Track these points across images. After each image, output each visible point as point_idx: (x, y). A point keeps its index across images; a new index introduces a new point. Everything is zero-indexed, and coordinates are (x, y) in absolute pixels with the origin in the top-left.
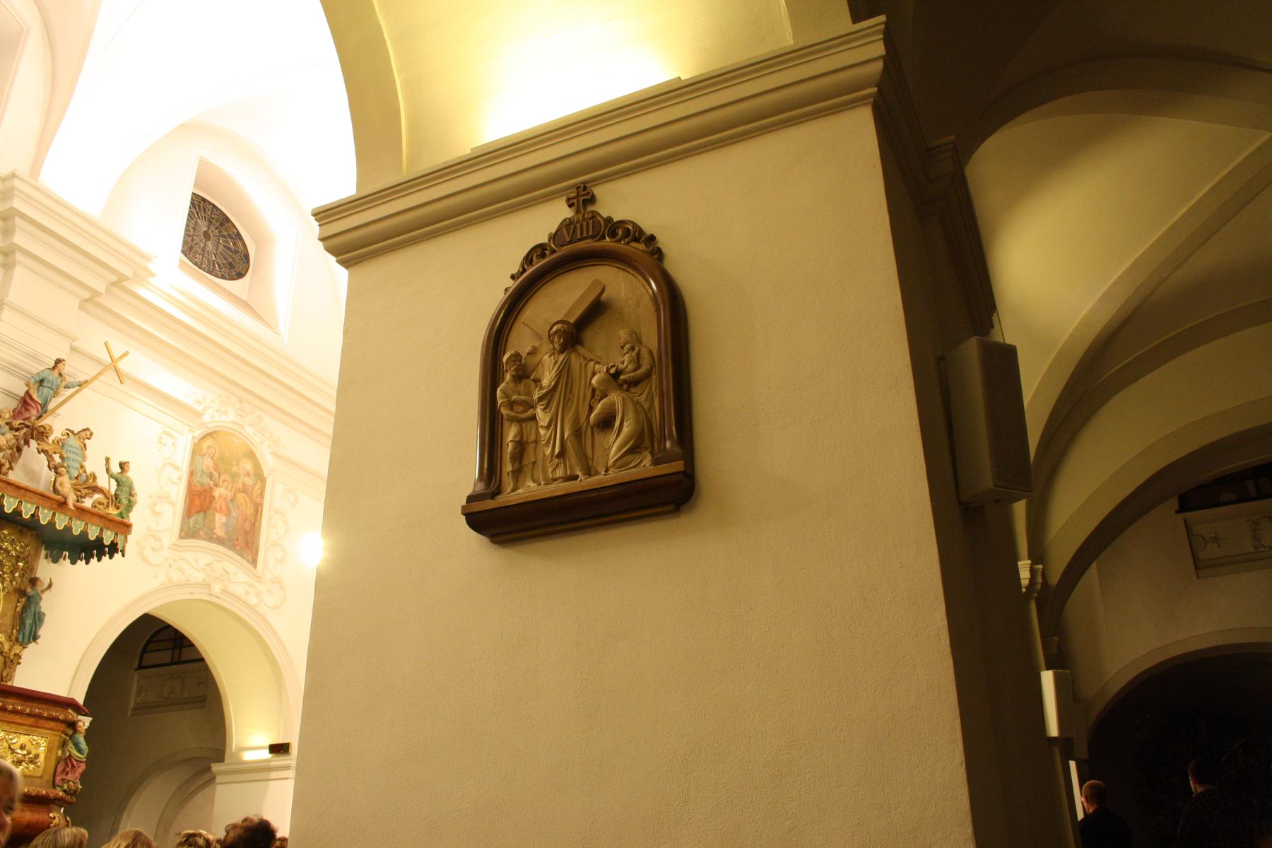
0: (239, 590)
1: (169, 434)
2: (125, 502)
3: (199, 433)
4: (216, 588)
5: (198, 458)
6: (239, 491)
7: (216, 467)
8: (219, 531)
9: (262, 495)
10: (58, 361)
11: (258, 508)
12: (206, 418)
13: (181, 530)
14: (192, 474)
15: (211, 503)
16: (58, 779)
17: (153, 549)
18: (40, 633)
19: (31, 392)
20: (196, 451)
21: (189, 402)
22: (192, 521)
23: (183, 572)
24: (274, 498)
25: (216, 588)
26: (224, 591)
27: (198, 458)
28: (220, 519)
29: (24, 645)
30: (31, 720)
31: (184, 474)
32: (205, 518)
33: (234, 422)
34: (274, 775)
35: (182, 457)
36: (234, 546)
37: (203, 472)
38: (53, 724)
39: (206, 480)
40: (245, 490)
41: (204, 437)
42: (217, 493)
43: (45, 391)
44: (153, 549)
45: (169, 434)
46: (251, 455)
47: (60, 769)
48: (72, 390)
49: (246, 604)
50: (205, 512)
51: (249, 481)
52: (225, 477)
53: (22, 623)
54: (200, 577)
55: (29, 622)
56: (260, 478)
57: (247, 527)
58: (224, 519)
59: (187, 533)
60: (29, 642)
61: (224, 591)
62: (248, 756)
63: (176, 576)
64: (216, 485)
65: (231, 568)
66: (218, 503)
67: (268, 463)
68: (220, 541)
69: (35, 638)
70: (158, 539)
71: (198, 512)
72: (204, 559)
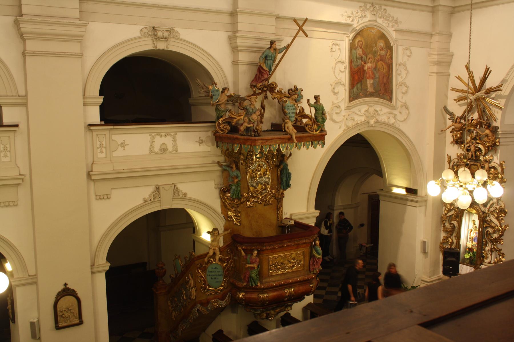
0: (383, 118)
1: (336, 44)
2: (320, 120)
3: (351, 36)
4: (372, 122)
5: (354, 51)
6: (378, 61)
7: (364, 53)
8: (370, 89)
9: (391, 58)
10: (272, 43)
11: (390, 67)
12: (355, 26)
13: (350, 97)
14: (351, 62)
15: (364, 75)
16: (311, 268)
17: (337, 113)
18: (290, 183)
19: (262, 65)
20: (352, 47)
21: (343, 20)
22: (355, 90)
23: (353, 120)
24: (399, 56)
25: (372, 122)
26: (377, 122)
27: (354, 51)
28: (369, 82)
29: (285, 189)
30: (296, 246)
31: (347, 64)
32: (361, 85)
33: (370, 21)
34: (409, 203)
35: (344, 55)
36: (379, 94)
37: (357, 58)
38: (305, 245)
39: (360, 62)
40: (381, 59)
41: (355, 37)
42: (366, 68)
43: (269, 62)
44: (337, 113)
45: (336, 44)
46: (383, 36)
47: (311, 263)
48: (282, 53)
49: (389, 125)
50: (361, 81)
51: (383, 53)
52: (370, 56)
53: (282, 180)
54: (363, 119)
55: (284, 179)
56: (389, 48)
57: (385, 80)
58: (372, 81)
59: (353, 97)
60: (286, 189)
61: (377, 122)
62: (395, 190)
63: (350, 124)
64: (365, 63)
65: (378, 108)
66: (368, 73)
67: (392, 36)
68: (371, 95)
69: (288, 186)
70: (338, 107)
71: (358, 83)
72: (364, 108)
